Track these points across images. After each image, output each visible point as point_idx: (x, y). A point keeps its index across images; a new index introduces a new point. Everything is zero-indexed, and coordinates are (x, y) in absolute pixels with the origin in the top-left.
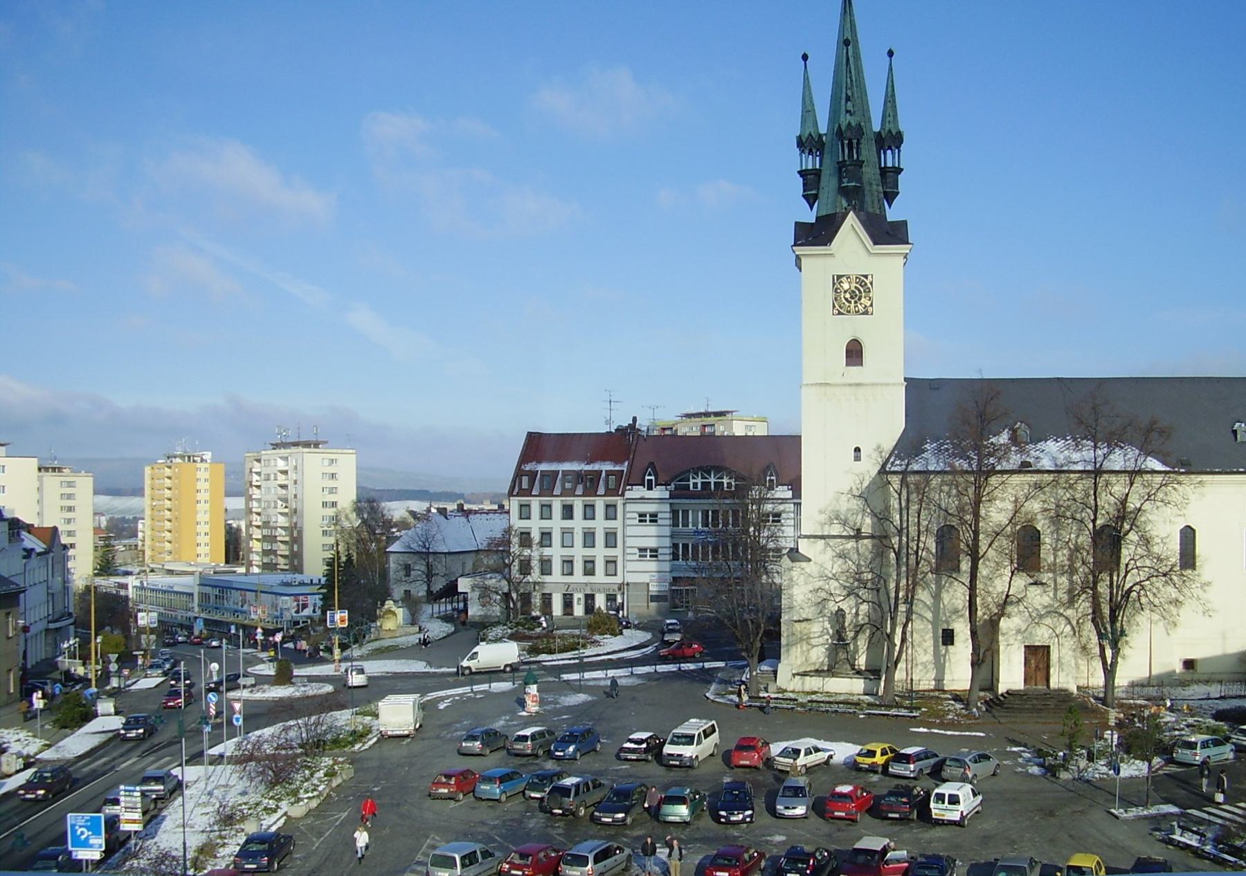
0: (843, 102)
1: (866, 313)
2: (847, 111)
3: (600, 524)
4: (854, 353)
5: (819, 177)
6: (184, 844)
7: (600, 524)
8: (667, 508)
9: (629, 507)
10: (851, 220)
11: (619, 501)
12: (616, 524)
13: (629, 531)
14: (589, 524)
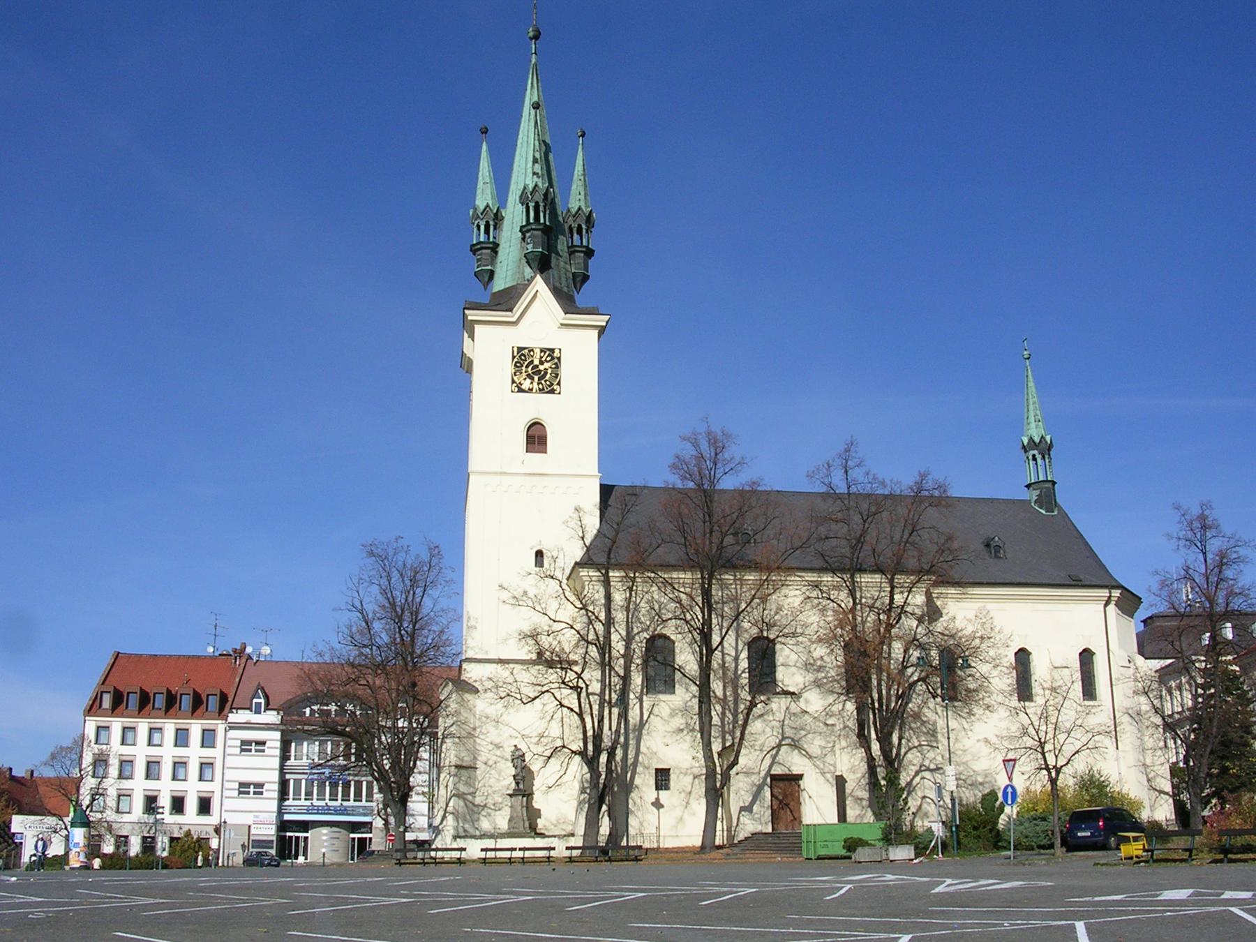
0: (530, 164)
1: (552, 392)
2: (534, 173)
3: (194, 753)
4: (536, 438)
5: (496, 253)
6: (658, 828)
7: (194, 753)
8: (278, 735)
9: (232, 733)
10: (539, 284)
11: (220, 726)
12: (214, 753)
13: (230, 761)
14: (181, 751)
